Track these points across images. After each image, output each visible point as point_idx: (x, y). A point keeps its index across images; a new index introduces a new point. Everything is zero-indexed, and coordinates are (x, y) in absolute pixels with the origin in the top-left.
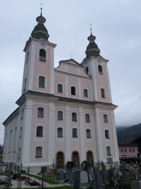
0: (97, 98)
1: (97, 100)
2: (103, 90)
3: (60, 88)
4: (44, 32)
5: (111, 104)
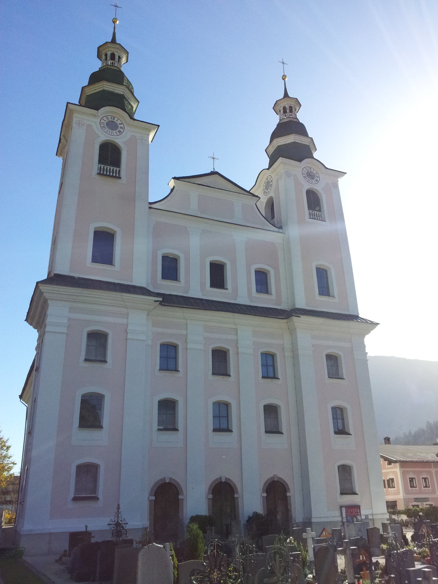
0: (303, 294)
1: (301, 304)
2: (322, 274)
3: (170, 268)
4: (118, 89)
5: (355, 317)
